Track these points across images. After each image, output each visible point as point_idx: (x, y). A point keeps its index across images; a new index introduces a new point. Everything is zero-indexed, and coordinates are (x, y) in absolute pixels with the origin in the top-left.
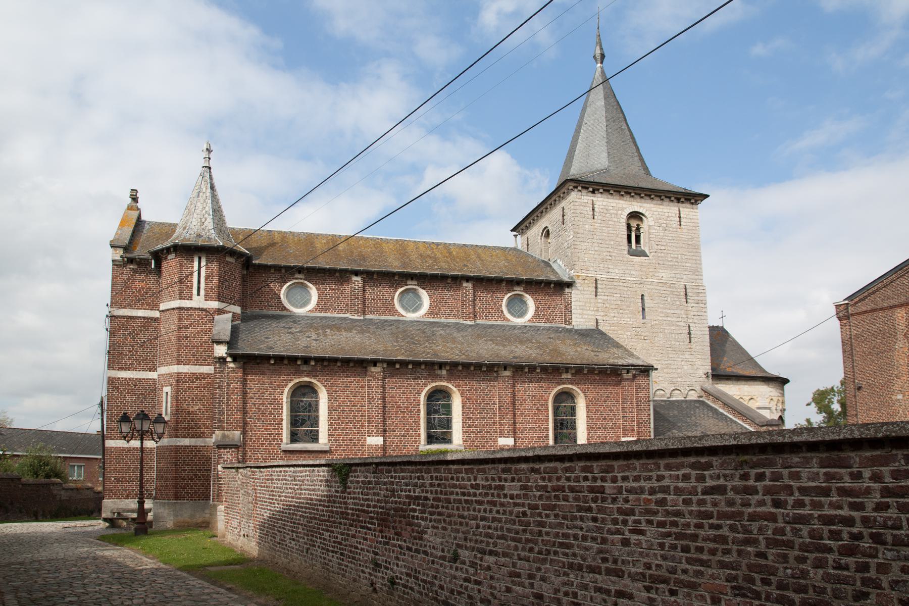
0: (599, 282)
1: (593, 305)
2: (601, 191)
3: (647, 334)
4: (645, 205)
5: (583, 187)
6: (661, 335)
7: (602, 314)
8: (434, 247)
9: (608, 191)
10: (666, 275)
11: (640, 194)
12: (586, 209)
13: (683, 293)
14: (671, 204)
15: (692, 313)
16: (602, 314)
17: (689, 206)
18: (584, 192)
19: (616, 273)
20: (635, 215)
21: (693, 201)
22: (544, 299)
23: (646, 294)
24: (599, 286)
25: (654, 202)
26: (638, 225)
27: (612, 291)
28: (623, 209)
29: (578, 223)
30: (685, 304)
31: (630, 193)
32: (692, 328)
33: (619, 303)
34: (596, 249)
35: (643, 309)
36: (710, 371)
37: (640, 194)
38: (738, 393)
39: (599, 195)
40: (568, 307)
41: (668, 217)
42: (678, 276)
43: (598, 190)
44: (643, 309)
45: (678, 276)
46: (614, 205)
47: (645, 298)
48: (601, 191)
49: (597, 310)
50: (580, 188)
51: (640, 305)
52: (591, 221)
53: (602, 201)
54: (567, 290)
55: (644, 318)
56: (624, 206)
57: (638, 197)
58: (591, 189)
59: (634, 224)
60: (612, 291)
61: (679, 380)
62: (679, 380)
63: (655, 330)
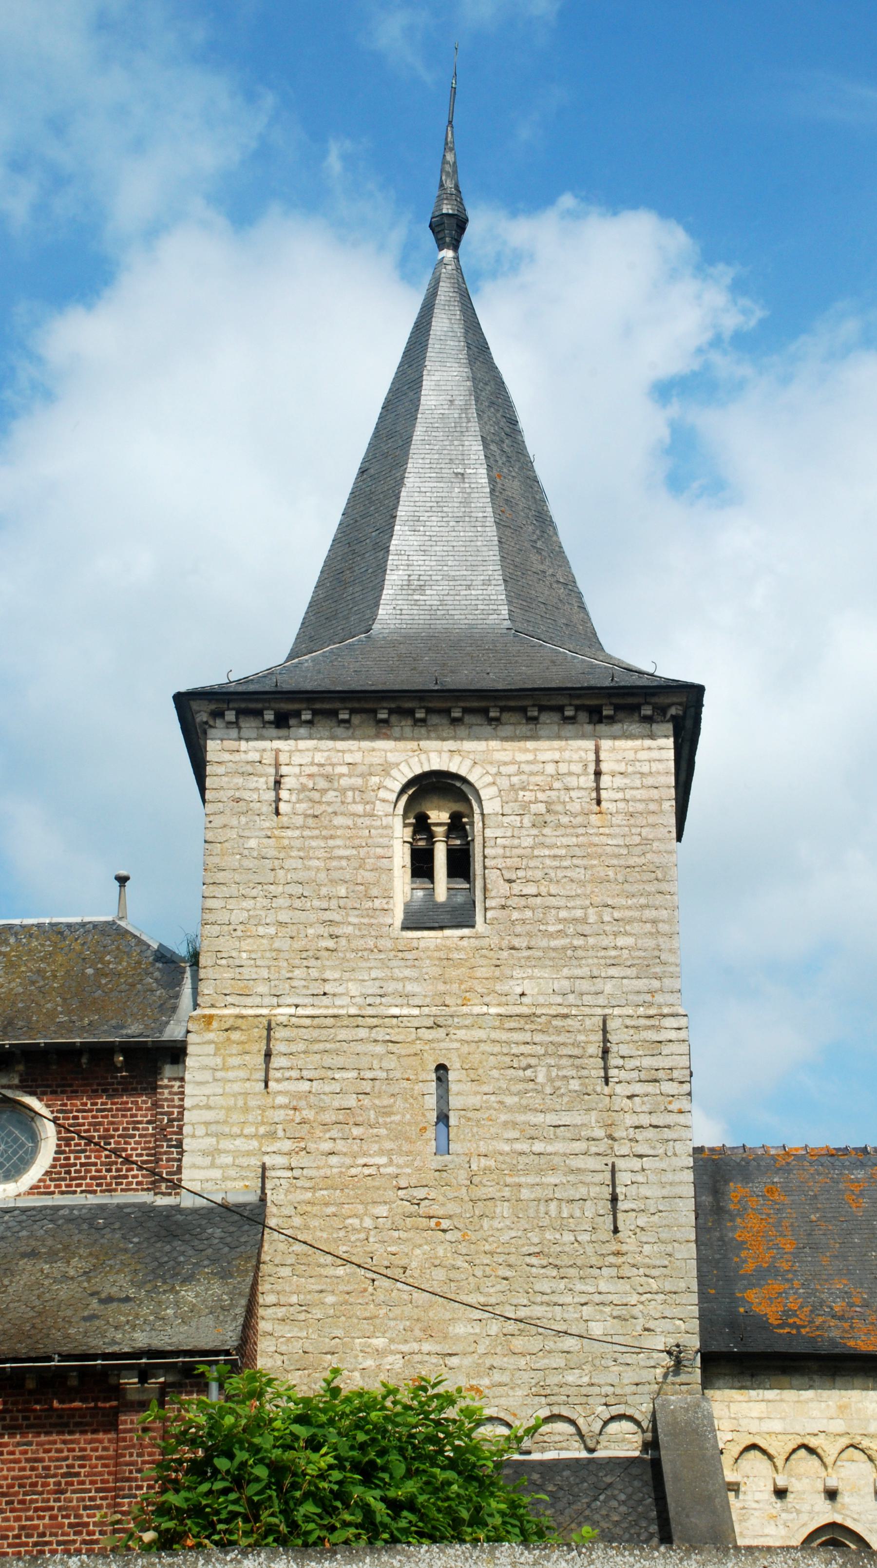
0: (279, 1033)
1: (254, 1116)
2: (306, 716)
3: (452, 1208)
4: (469, 745)
5: (617, 708)
6: (504, 1209)
7: (287, 1145)
8: (133, 942)
9: (334, 713)
10: (535, 985)
11: (447, 711)
12: (253, 782)
13: (594, 1049)
14: (569, 729)
15: (630, 1120)
16: (287, 1145)
17: (635, 728)
18: (249, 725)
19: (350, 994)
20: (432, 786)
21: (647, 711)
22: (89, 1110)
23: (454, 1064)
24: (278, 1047)
25: (507, 730)
26: (456, 818)
27: (328, 1061)
28: (386, 769)
29: (222, 835)
30: (600, 1087)
31: (411, 713)
32: (623, 1178)
33: (351, 1101)
34: (283, 917)
35: (443, 1118)
36: (694, 1342)
37: (447, 711)
38: (838, 1426)
39: (303, 731)
40: (169, 1134)
41: (558, 776)
42: (585, 986)
43: (297, 714)
44: (443, 1118)
45: (585, 986)
46: (357, 757)
47: (452, 1076)
48: (306, 716)
49: (272, 1135)
50: (230, 716)
51: (431, 1102)
52: (271, 822)
53: (304, 754)
54: (168, 1070)
55: (444, 1149)
56: (392, 758)
57: (514, 717)
58: (269, 716)
59: (439, 816)
60: (328, 1061)
61: (571, 1378)
62: (571, 1378)
63: (481, 1192)
